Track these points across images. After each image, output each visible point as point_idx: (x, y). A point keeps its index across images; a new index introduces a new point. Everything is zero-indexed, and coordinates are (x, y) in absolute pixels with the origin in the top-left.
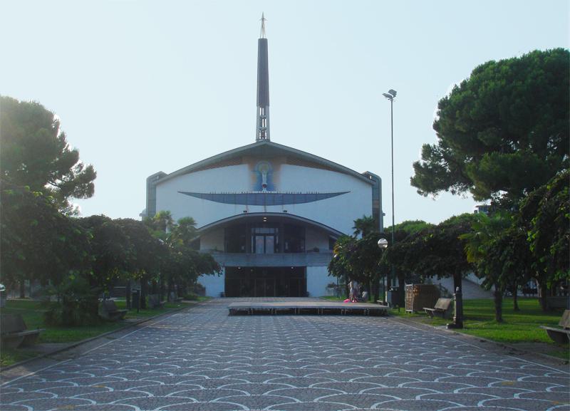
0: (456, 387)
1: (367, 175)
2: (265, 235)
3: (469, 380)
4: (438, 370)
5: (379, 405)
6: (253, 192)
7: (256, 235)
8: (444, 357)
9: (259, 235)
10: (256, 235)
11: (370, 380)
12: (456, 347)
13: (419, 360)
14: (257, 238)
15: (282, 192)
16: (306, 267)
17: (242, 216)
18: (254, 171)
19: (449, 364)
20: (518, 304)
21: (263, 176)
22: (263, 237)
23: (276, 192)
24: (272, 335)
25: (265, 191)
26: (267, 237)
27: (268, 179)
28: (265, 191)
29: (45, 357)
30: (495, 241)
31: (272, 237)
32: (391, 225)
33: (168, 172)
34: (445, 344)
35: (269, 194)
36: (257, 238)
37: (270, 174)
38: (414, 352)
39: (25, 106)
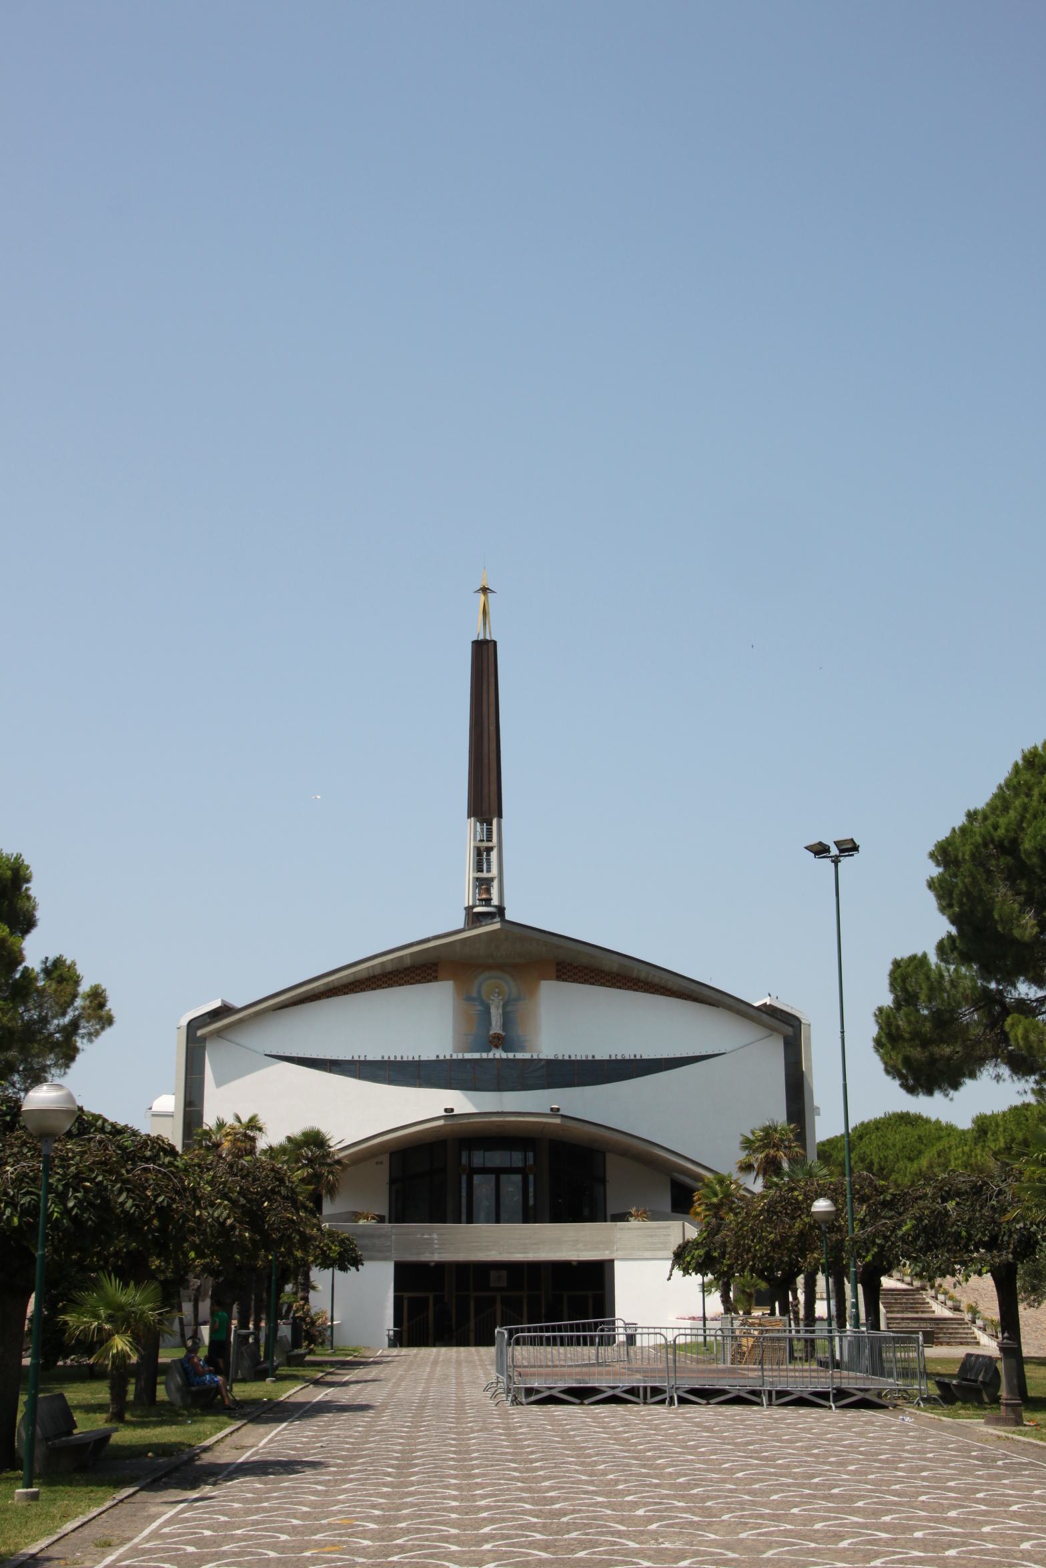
0: (987, 1523)
1: (771, 1011)
2: (498, 1172)
3: (1015, 1515)
4: (955, 1499)
5: (852, 1543)
6: (468, 1056)
7: (473, 1171)
8: (970, 1480)
9: (484, 1171)
10: (473, 1171)
11: (829, 1510)
12: (1000, 1463)
13: (919, 1483)
14: (477, 1179)
15: (542, 1056)
16: (612, 1261)
17: (441, 1122)
18: (469, 999)
19: (979, 1491)
20: (1027, 1374)
21: (493, 1011)
22: (492, 1177)
23: (527, 1056)
24: (500, 1450)
25: (499, 1054)
26: (503, 1177)
27: (507, 1021)
28: (499, 1054)
29: (166, 1475)
30: (913, 1355)
31: (518, 1178)
32: (840, 1131)
33: (238, 1001)
34: (976, 1458)
35: (508, 1060)
36: (477, 1179)
37: (509, 1008)
38: (911, 1470)
39: (33, 916)
